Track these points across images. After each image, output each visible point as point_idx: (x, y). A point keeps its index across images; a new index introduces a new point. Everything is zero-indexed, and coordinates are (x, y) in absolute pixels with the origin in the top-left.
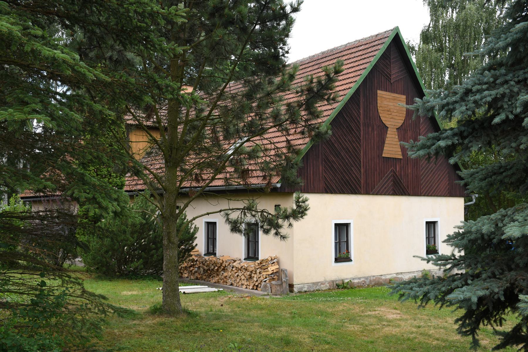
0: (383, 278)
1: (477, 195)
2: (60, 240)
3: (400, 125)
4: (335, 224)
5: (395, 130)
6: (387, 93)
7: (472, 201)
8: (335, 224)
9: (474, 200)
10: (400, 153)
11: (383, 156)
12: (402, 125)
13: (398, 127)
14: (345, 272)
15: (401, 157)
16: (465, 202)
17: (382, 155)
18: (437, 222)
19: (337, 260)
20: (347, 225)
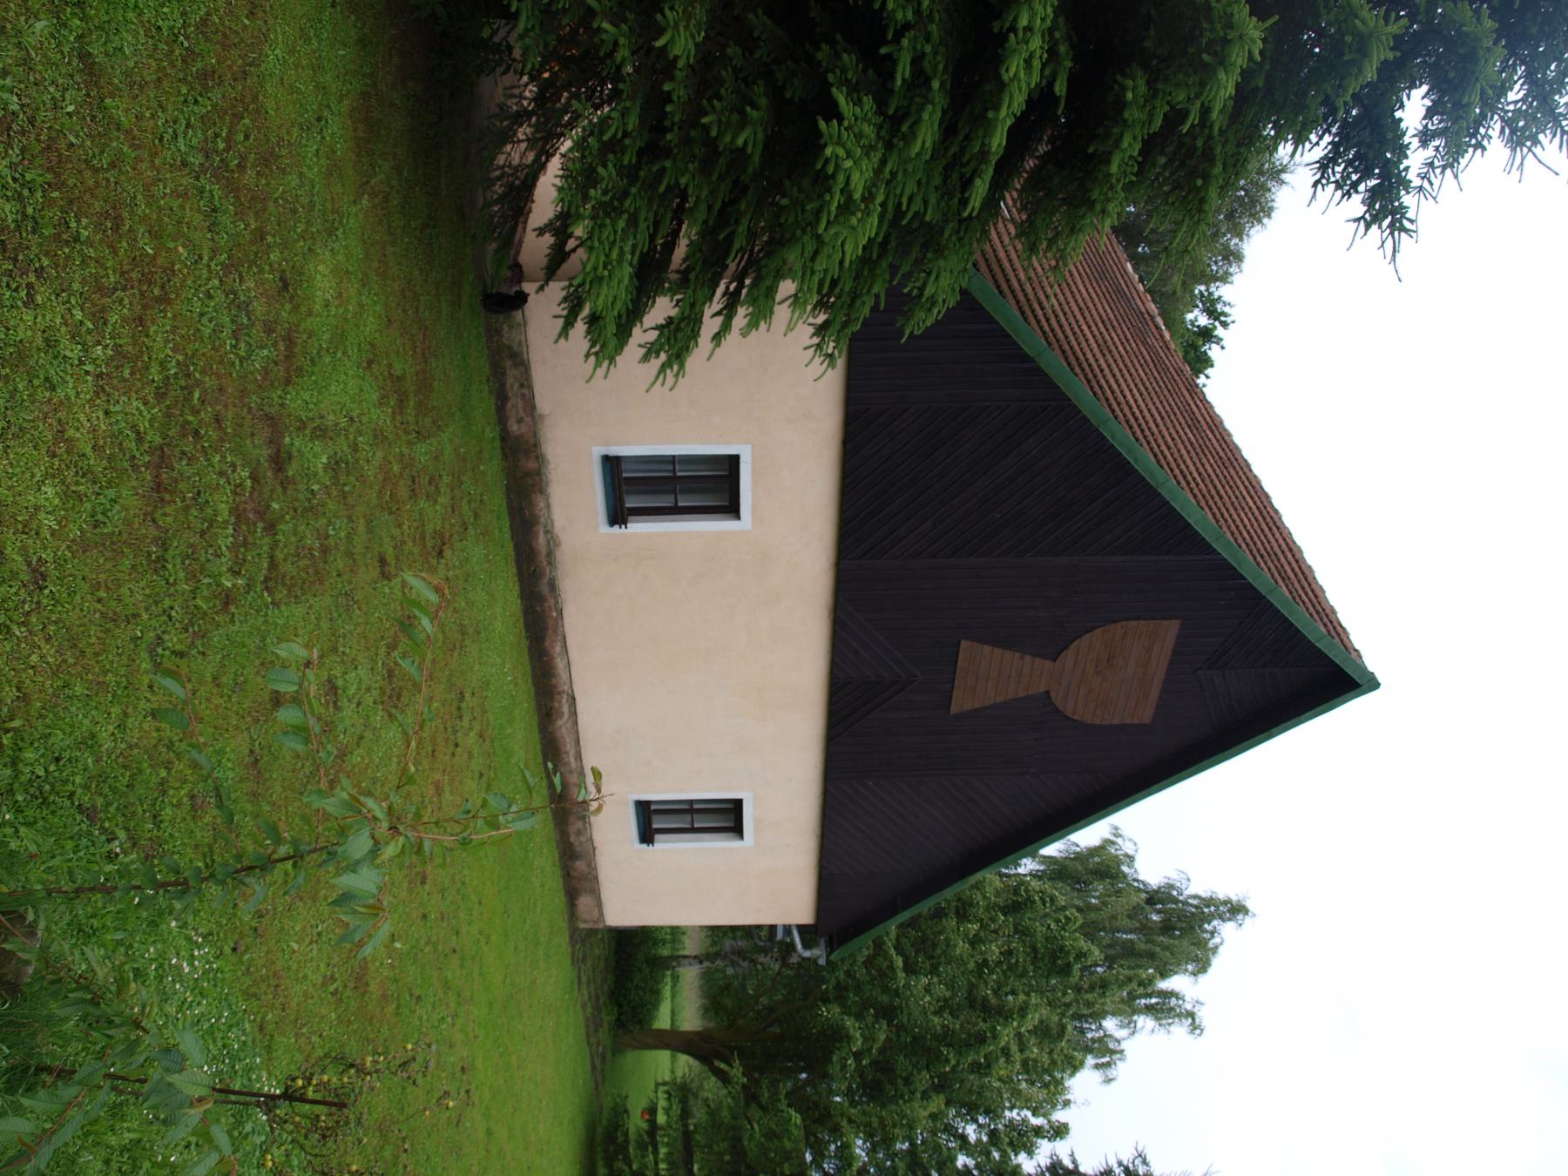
0: (558, 649)
1: (822, 962)
2: (218, 420)
3: (1058, 703)
4: (740, 801)
5: (1042, 689)
6: (1164, 665)
7: (806, 946)
8: (740, 801)
9: (807, 954)
10: (968, 706)
11: (964, 644)
12: (1057, 710)
13: (1053, 695)
14: (574, 501)
15: (954, 709)
16: (801, 928)
17: (967, 638)
18: (741, 837)
19: (612, 464)
20: (737, 829)
